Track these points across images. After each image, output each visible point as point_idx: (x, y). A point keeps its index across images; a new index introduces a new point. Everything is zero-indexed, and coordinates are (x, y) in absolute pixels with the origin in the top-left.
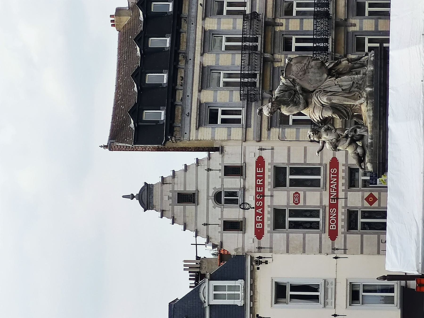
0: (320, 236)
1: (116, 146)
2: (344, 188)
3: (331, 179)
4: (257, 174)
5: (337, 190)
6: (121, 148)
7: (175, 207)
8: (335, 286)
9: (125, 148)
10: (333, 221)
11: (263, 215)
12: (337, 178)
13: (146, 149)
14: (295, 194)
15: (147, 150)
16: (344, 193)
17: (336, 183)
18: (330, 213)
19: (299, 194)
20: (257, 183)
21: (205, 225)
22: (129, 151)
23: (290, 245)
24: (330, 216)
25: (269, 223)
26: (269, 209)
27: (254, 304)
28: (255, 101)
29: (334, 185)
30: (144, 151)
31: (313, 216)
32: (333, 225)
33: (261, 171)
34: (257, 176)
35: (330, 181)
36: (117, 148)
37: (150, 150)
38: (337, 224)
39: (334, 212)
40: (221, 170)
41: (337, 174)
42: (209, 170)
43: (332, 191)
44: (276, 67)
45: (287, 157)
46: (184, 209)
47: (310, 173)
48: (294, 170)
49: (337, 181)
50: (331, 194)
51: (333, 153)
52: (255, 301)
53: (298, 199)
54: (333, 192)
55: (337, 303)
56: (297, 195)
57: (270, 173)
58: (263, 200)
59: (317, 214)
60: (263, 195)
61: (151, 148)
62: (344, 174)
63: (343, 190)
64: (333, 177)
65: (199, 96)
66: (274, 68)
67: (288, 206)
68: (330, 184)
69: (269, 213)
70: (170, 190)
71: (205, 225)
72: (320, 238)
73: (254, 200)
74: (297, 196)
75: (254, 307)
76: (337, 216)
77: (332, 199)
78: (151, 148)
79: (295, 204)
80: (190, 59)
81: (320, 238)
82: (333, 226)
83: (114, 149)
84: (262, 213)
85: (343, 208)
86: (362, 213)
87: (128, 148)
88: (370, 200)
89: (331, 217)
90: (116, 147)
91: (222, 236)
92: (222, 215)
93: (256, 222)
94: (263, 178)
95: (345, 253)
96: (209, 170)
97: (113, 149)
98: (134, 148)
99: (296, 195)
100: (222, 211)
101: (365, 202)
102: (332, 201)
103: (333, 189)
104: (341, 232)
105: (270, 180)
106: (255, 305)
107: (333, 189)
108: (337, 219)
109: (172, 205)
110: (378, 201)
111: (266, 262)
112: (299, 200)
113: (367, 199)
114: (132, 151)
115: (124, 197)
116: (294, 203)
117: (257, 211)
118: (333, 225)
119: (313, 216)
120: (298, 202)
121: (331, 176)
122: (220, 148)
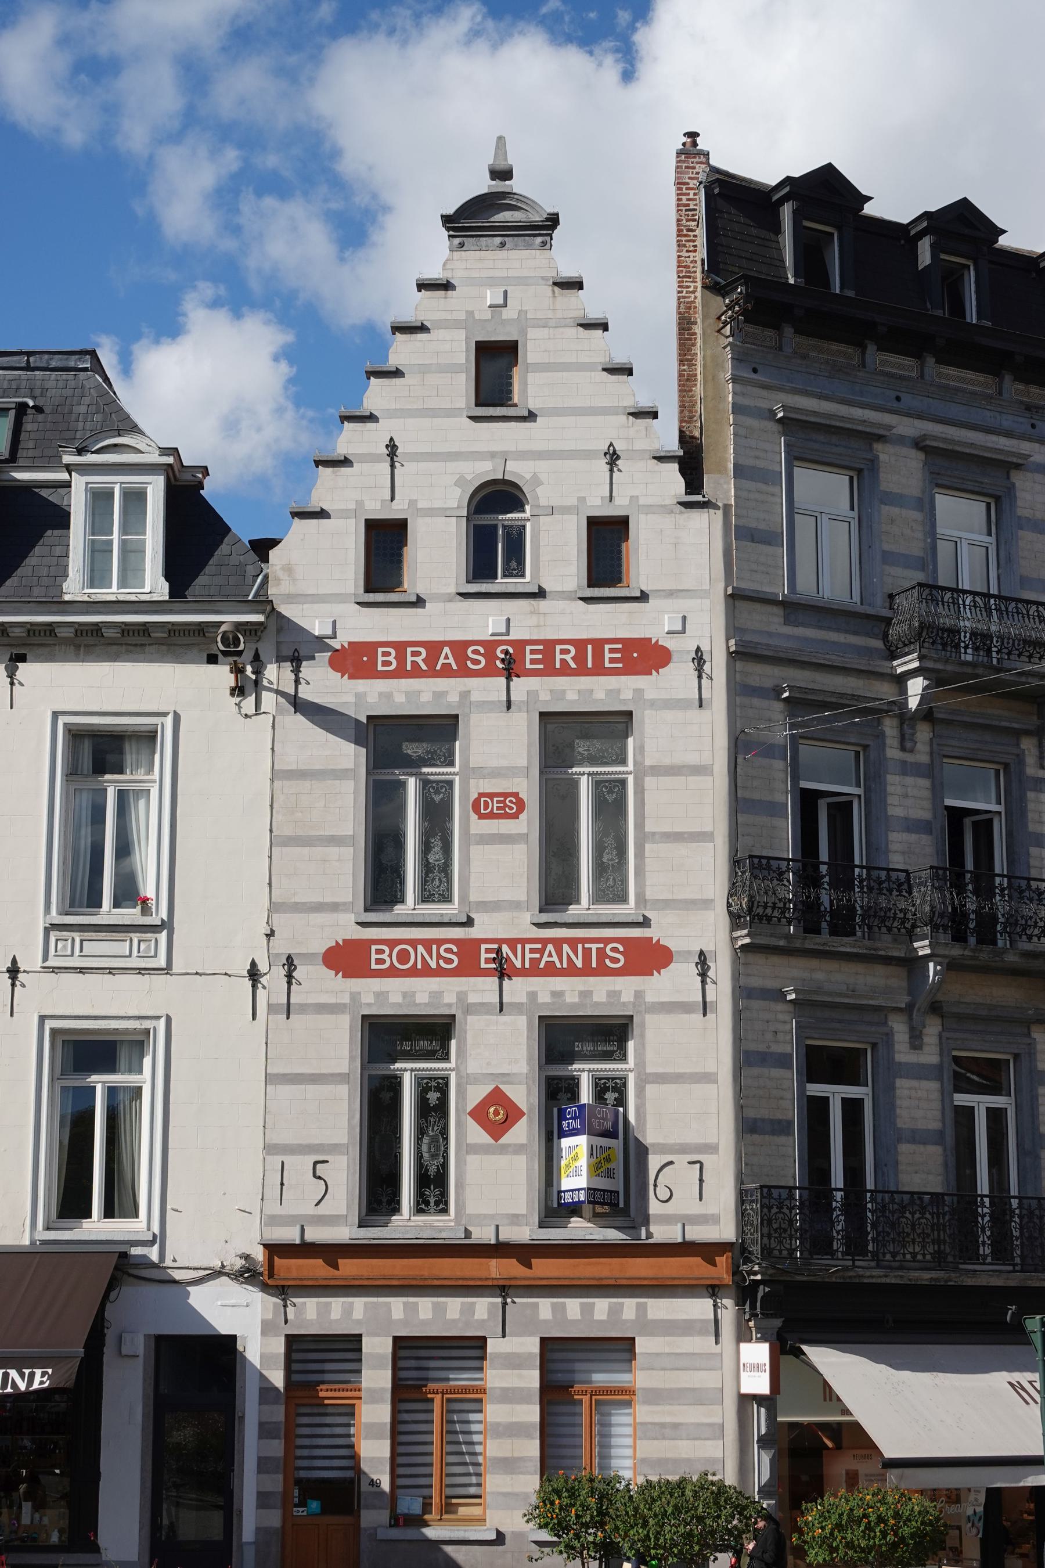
0: (345, 904)
1: (695, 171)
2: (544, 998)
3: (580, 946)
4: (598, 644)
5: (534, 970)
6: (688, 192)
7: (461, 334)
8: (140, 971)
9: (688, 205)
10: (403, 957)
11: (433, 673)
12: (587, 971)
13: (685, 280)
14: (514, 800)
15: (682, 282)
16: (524, 1000)
17: (565, 966)
18: (440, 942)
19: (515, 816)
20: (558, 648)
21: (392, 448)
22: (678, 220)
23: (307, 784)
24: (427, 944)
25: (396, 700)
26: (454, 698)
27: (66, 642)
28: (889, 649)
29: (555, 958)
30: (678, 272)
31: (427, 875)
32: (390, 956)
33: (610, 662)
34: (590, 647)
35: (573, 943)
36: (687, 176)
37: (682, 292)
38: (392, 972)
39: (441, 962)
40: (612, 504)
41: (603, 971)
42: (613, 458)
43: (532, 951)
44: (1023, 746)
45: (667, 761)
46: (451, 369)
47: (605, 860)
48: (614, 795)
49: (571, 971)
50: (519, 946)
51: (689, 952)
52: (80, 646)
53: (495, 811)
54: (528, 956)
55: (64, 977)
56: (511, 808)
57: (600, 695)
58: (488, 672)
59: (433, 894)
60: (511, 668)
61: (689, 297)
62: (600, 997)
63: (533, 995)
64: (587, 952)
65: (901, 440)
66: (1018, 734)
67: (468, 772)
68: (558, 943)
69: (439, 695)
70: (526, 312)
71: (392, 448)
72: (335, 907)
73: (492, 635)
74: (507, 809)
75: (55, 645)
76: (426, 971)
77: (499, 951)
78: (689, 297)
79: (476, 800)
80: (1033, 426)
81: (335, 907)
82: (385, 956)
83: (684, 165)
84: (438, 668)
85: (462, 996)
86: (440, 1081)
87: (688, 215)
88: (492, 1110)
89: (420, 948)
90: (692, 173)
91: (345, 514)
92: (431, 512)
93: (401, 647)
94: (582, 671)
95: (271, 1008)
96: (613, 458)
97: (684, 162)
98: (689, 236)
99: (511, 801)
100: (448, 513)
101: (488, 1089)
102: (488, 951)
103: (538, 956)
104: (358, 990)
105: (571, 696)
106: (63, 647)
107: (538, 956)
108: (413, 972)
109: (469, 321)
110: (492, 1144)
111: (238, 691)
112: (491, 816)
113: (497, 1097)
114: (679, 231)
115: (501, 140)
116: (481, 795)
117: (446, 650)
118: (389, 958)
119: (427, 875)
120: (482, 811)
121: (594, 947)
122: (698, 498)
